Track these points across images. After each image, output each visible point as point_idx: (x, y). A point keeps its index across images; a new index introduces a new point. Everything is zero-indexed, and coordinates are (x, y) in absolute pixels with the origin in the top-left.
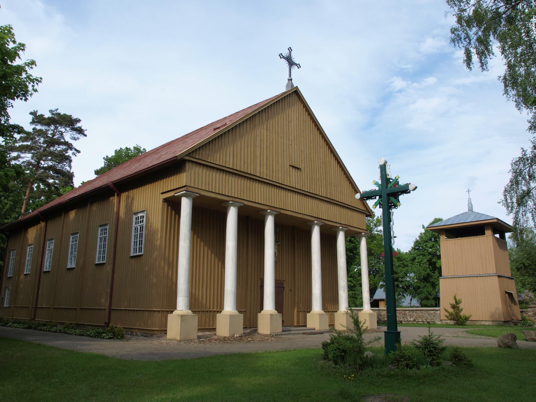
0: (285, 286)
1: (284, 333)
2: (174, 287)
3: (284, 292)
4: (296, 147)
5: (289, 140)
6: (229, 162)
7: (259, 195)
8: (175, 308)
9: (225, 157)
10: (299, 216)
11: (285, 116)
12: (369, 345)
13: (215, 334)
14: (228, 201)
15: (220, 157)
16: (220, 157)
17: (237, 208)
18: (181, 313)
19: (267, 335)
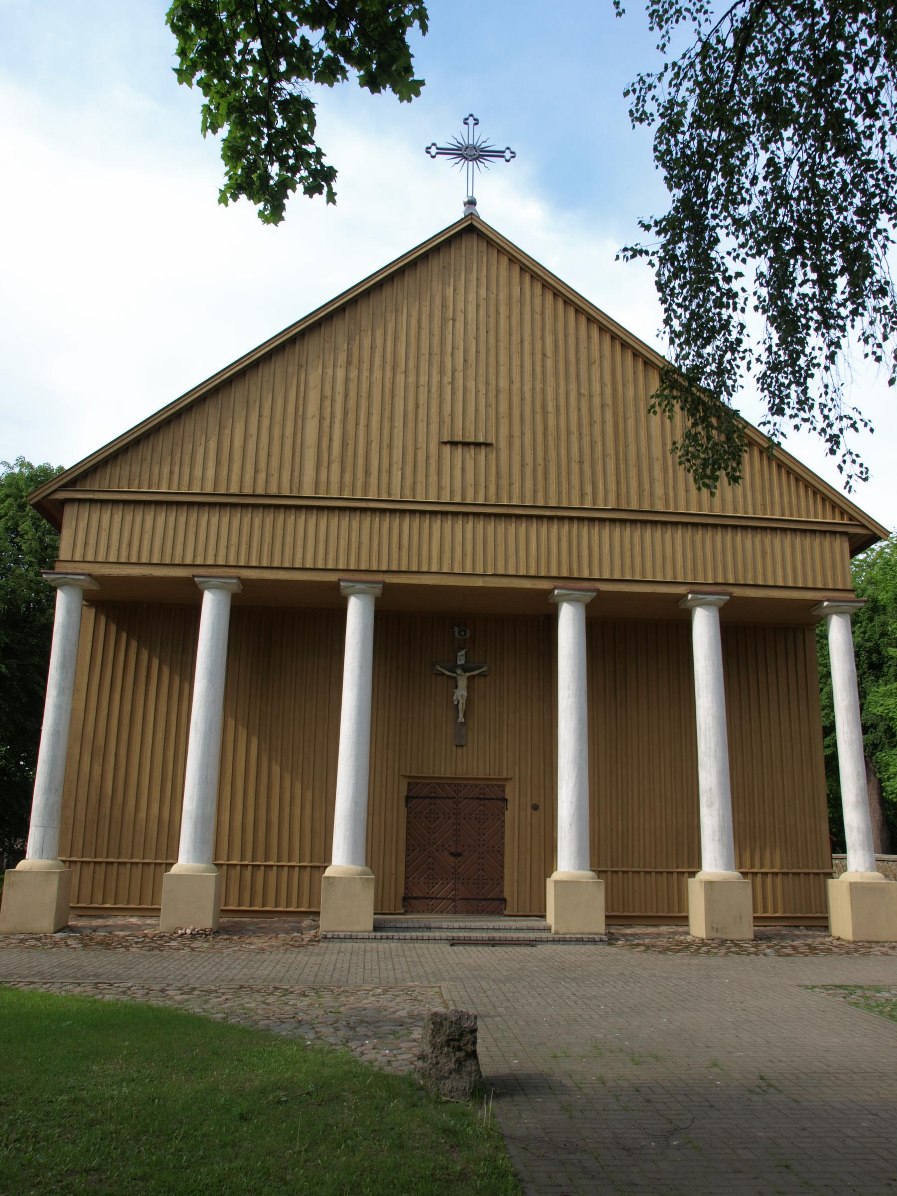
0: (508, 795)
1: (378, 934)
2: (696, 821)
3: (508, 813)
4: (471, 384)
5: (442, 372)
6: (204, 479)
7: (301, 550)
8: (700, 866)
9: (199, 468)
10: (479, 582)
11: (426, 311)
12: (227, 1005)
13: (688, 933)
14: (336, 586)
15: (171, 473)
16: (171, 473)
17: (848, 617)
18: (856, 878)
19: (849, 942)
